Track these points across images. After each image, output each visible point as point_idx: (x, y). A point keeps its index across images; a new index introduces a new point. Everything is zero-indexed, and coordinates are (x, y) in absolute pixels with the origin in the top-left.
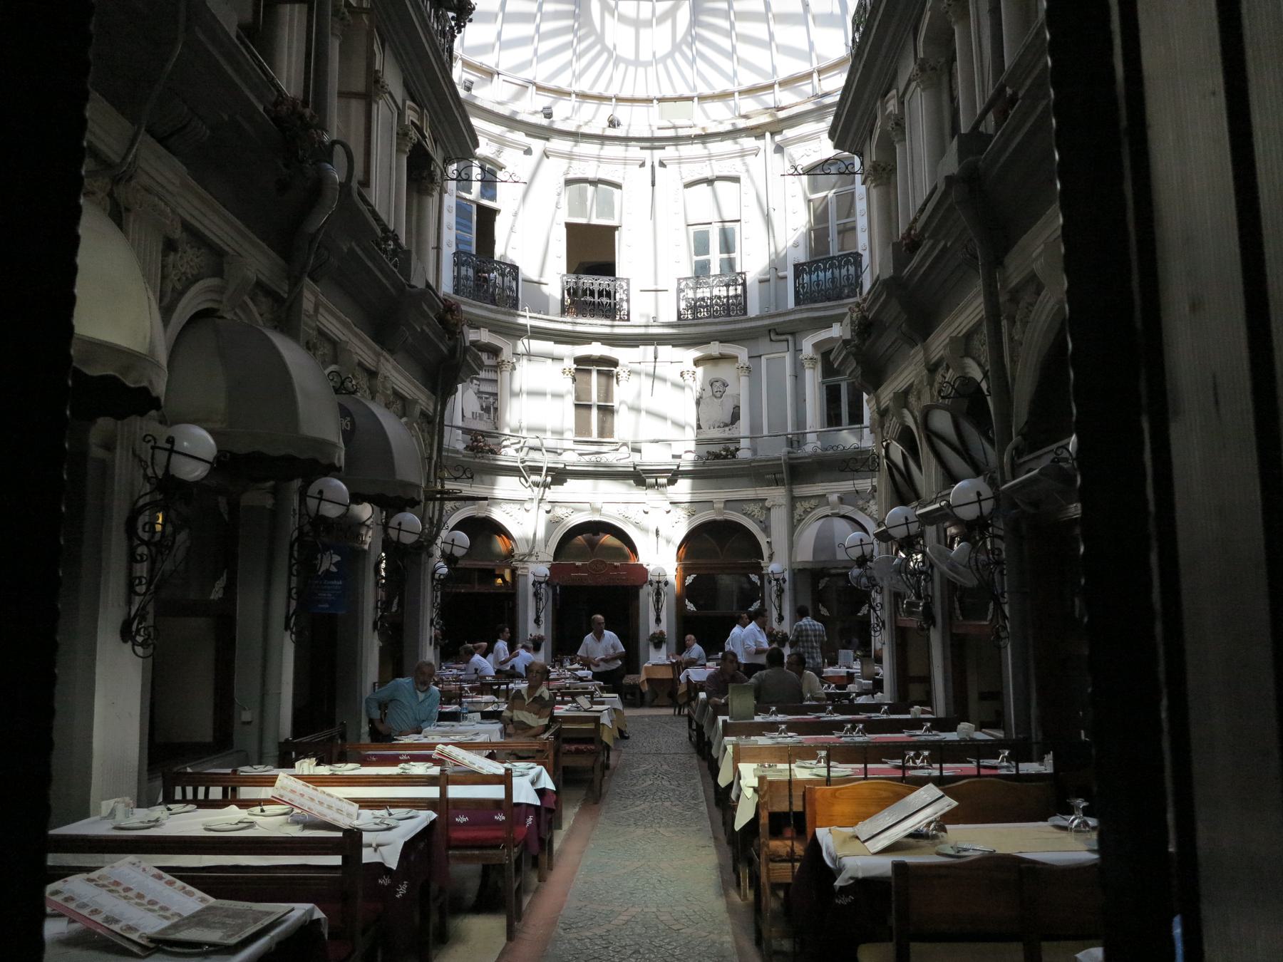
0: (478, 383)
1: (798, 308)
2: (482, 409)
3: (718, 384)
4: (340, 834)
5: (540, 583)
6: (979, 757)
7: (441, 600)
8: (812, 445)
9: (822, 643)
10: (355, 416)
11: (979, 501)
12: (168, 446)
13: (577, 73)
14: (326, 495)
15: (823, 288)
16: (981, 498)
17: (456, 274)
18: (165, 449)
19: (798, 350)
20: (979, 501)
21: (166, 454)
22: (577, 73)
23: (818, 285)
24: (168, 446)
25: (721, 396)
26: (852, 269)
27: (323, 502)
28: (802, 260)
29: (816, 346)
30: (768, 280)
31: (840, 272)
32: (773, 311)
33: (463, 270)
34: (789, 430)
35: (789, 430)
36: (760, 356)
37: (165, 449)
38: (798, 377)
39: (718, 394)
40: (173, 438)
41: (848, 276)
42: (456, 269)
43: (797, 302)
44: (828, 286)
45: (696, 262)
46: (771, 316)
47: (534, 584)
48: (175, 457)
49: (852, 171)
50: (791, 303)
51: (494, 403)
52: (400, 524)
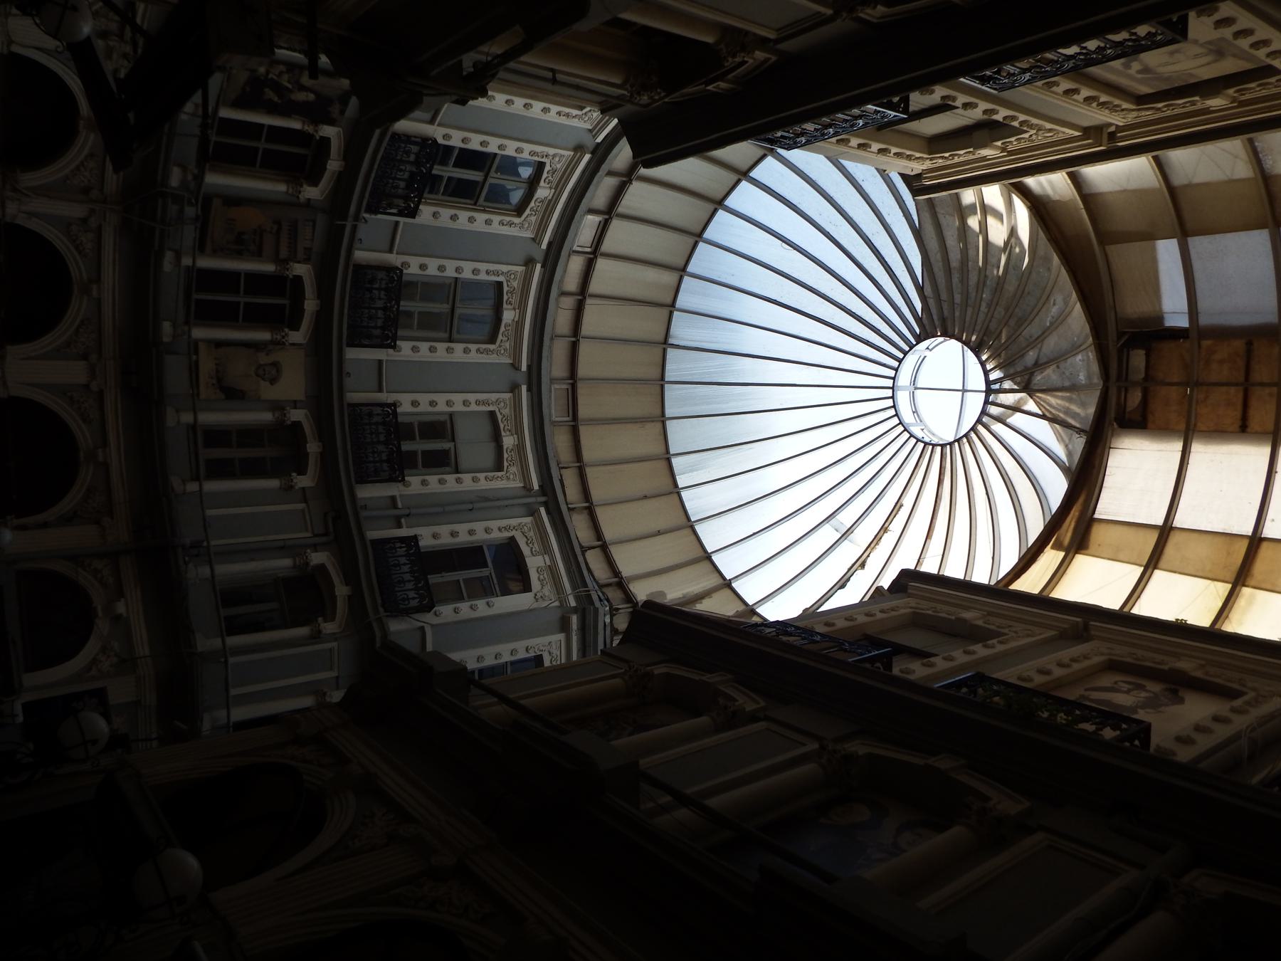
1: (368, 544)
4: (311, 97)
7: (970, 148)
8: (196, 573)
10: (612, 601)
15: (397, 589)
17: (413, 139)
19: (315, 548)
23: (404, 600)
25: (258, 375)
26: (414, 603)
28: (421, 543)
29: (322, 567)
30: (395, 507)
31: (412, 590)
32: (364, 514)
33: (415, 149)
34: (213, 543)
35: (213, 543)
36: (306, 501)
38: (283, 549)
41: (399, 565)
42: (419, 140)
43: (374, 542)
44: (399, 594)
45: (421, 438)
46: (356, 514)
50: (373, 534)
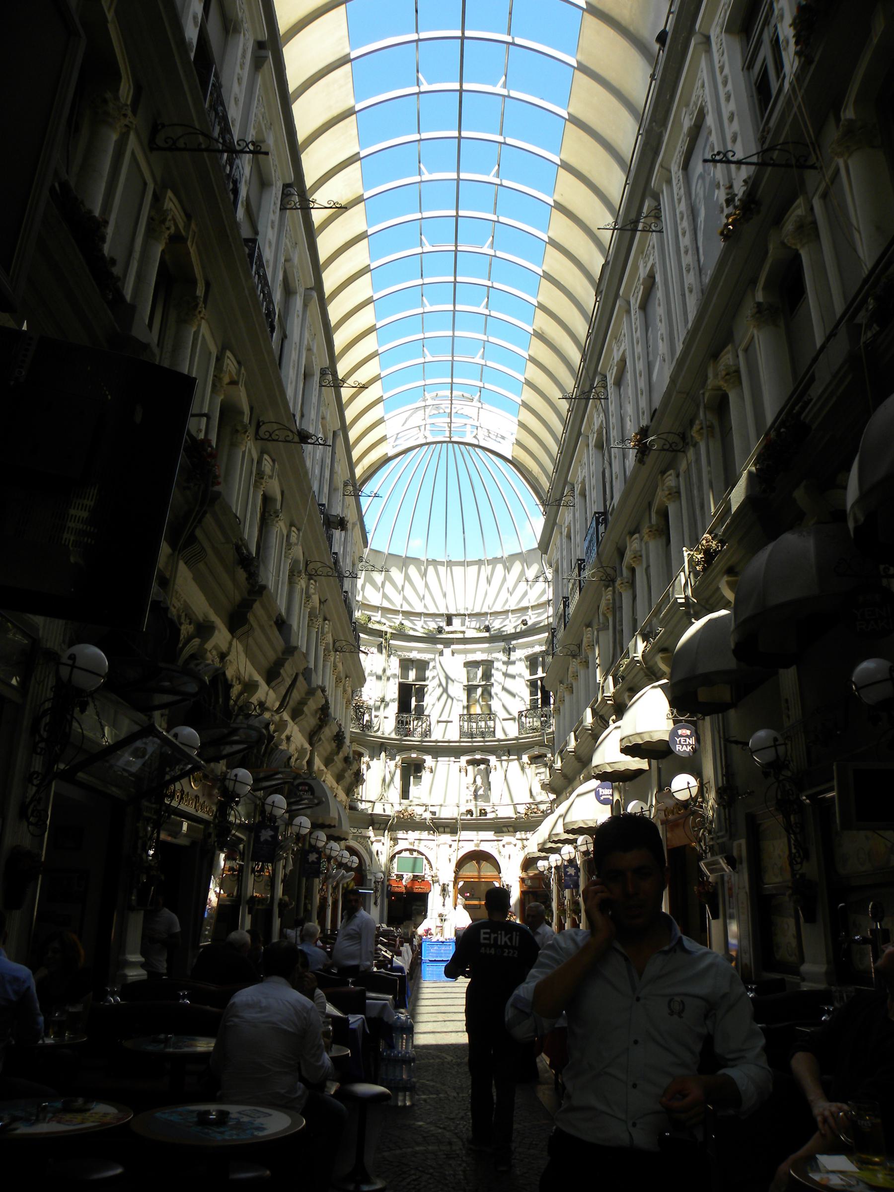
5: (378, 882)
6: (464, 638)
9: (160, 602)
11: (775, 746)
12: (70, 662)
13: (511, 590)
14: (79, 662)
16: (777, 743)
18: (68, 665)
20: (775, 746)
21: (69, 668)
22: (511, 590)
24: (70, 662)
27: (75, 670)
37: (68, 665)
40: (74, 655)
47: (375, 882)
48: (75, 670)
49: (675, 448)
52: (273, 802)
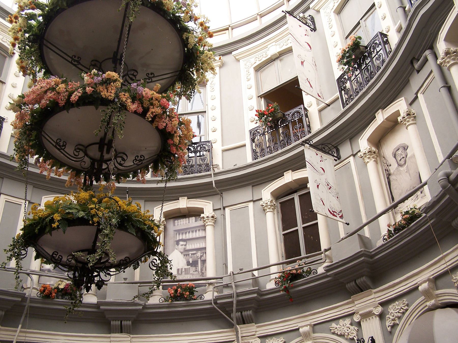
0: (184, 243)
2: (188, 263)
3: (399, 152)
39: (402, 162)
51: (201, 256)
